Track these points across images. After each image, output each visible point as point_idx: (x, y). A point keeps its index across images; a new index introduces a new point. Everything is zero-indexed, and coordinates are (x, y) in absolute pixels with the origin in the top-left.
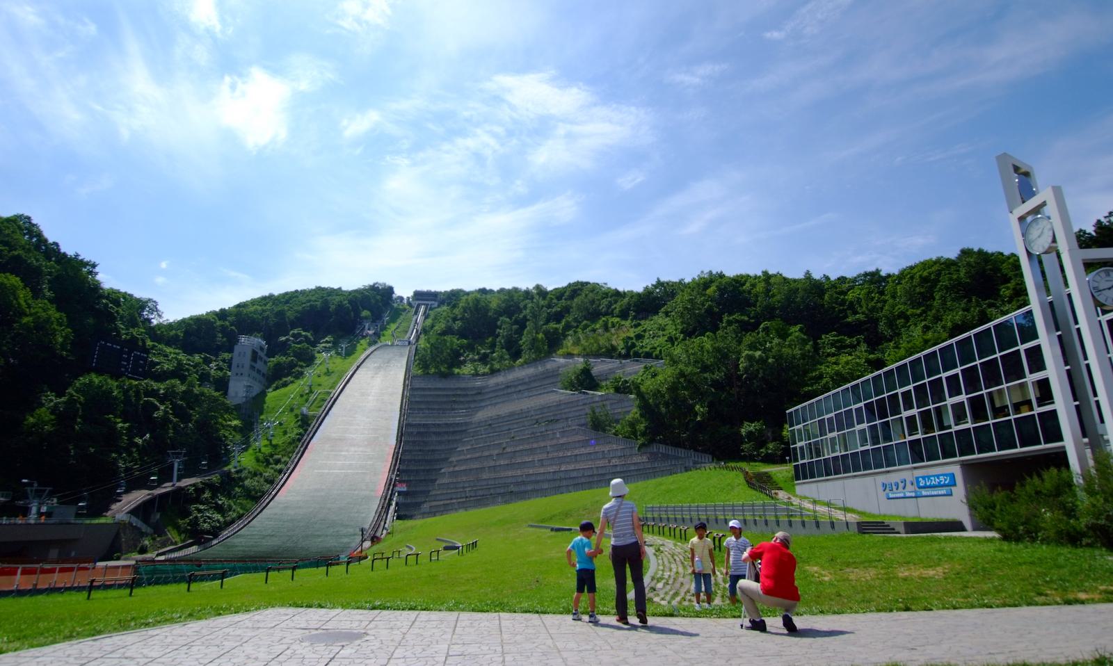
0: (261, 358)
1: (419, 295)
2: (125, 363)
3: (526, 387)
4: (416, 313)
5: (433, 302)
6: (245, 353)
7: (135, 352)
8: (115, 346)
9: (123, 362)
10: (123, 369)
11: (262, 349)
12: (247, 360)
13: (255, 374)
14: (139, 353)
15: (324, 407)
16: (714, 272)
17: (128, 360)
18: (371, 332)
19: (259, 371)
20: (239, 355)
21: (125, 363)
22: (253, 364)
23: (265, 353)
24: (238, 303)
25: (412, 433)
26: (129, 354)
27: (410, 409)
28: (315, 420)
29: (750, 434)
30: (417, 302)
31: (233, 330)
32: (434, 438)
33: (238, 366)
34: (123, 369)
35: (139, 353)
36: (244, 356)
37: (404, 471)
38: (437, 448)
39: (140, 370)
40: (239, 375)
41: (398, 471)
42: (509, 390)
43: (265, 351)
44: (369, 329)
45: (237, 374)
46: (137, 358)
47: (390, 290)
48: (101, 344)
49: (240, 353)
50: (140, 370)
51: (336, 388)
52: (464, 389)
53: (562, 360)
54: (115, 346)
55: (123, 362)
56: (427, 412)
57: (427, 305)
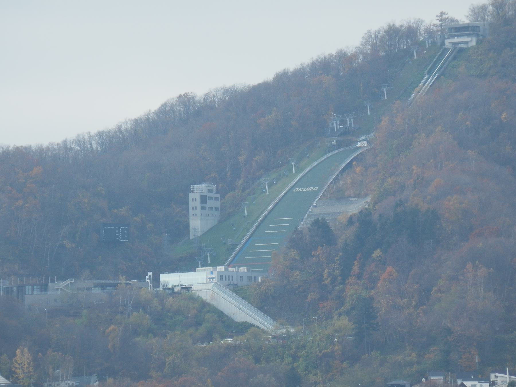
2: (118, 235)
6: (196, 199)
9: (117, 235)
10: (118, 238)
21: (118, 235)
22: (204, 205)
34: (118, 238)
45: (193, 215)
55: (117, 235)
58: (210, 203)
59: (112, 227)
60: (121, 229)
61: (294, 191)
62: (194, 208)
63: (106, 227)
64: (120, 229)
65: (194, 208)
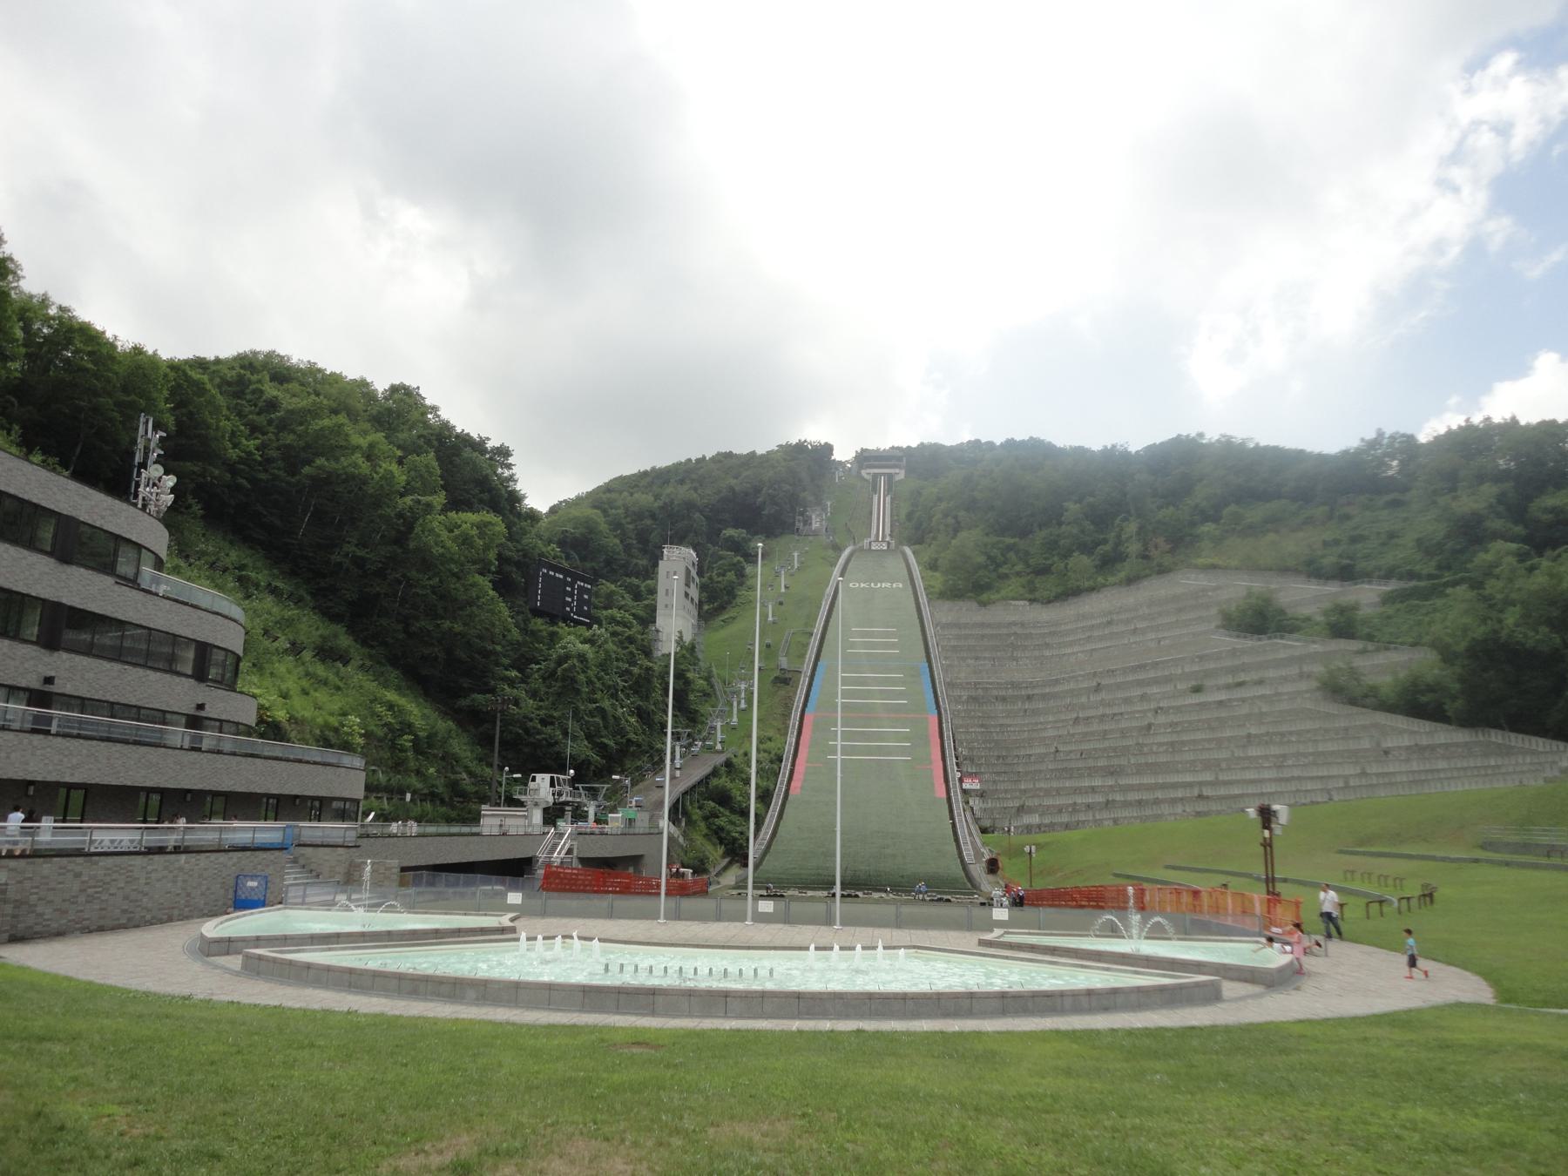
2: (570, 600)
5: (897, 471)
8: (552, 573)
10: (568, 609)
17: (571, 595)
25: (960, 697)
34: (568, 609)
42: (1115, 629)
56: (973, 661)
59: (560, 573)
61: (851, 585)
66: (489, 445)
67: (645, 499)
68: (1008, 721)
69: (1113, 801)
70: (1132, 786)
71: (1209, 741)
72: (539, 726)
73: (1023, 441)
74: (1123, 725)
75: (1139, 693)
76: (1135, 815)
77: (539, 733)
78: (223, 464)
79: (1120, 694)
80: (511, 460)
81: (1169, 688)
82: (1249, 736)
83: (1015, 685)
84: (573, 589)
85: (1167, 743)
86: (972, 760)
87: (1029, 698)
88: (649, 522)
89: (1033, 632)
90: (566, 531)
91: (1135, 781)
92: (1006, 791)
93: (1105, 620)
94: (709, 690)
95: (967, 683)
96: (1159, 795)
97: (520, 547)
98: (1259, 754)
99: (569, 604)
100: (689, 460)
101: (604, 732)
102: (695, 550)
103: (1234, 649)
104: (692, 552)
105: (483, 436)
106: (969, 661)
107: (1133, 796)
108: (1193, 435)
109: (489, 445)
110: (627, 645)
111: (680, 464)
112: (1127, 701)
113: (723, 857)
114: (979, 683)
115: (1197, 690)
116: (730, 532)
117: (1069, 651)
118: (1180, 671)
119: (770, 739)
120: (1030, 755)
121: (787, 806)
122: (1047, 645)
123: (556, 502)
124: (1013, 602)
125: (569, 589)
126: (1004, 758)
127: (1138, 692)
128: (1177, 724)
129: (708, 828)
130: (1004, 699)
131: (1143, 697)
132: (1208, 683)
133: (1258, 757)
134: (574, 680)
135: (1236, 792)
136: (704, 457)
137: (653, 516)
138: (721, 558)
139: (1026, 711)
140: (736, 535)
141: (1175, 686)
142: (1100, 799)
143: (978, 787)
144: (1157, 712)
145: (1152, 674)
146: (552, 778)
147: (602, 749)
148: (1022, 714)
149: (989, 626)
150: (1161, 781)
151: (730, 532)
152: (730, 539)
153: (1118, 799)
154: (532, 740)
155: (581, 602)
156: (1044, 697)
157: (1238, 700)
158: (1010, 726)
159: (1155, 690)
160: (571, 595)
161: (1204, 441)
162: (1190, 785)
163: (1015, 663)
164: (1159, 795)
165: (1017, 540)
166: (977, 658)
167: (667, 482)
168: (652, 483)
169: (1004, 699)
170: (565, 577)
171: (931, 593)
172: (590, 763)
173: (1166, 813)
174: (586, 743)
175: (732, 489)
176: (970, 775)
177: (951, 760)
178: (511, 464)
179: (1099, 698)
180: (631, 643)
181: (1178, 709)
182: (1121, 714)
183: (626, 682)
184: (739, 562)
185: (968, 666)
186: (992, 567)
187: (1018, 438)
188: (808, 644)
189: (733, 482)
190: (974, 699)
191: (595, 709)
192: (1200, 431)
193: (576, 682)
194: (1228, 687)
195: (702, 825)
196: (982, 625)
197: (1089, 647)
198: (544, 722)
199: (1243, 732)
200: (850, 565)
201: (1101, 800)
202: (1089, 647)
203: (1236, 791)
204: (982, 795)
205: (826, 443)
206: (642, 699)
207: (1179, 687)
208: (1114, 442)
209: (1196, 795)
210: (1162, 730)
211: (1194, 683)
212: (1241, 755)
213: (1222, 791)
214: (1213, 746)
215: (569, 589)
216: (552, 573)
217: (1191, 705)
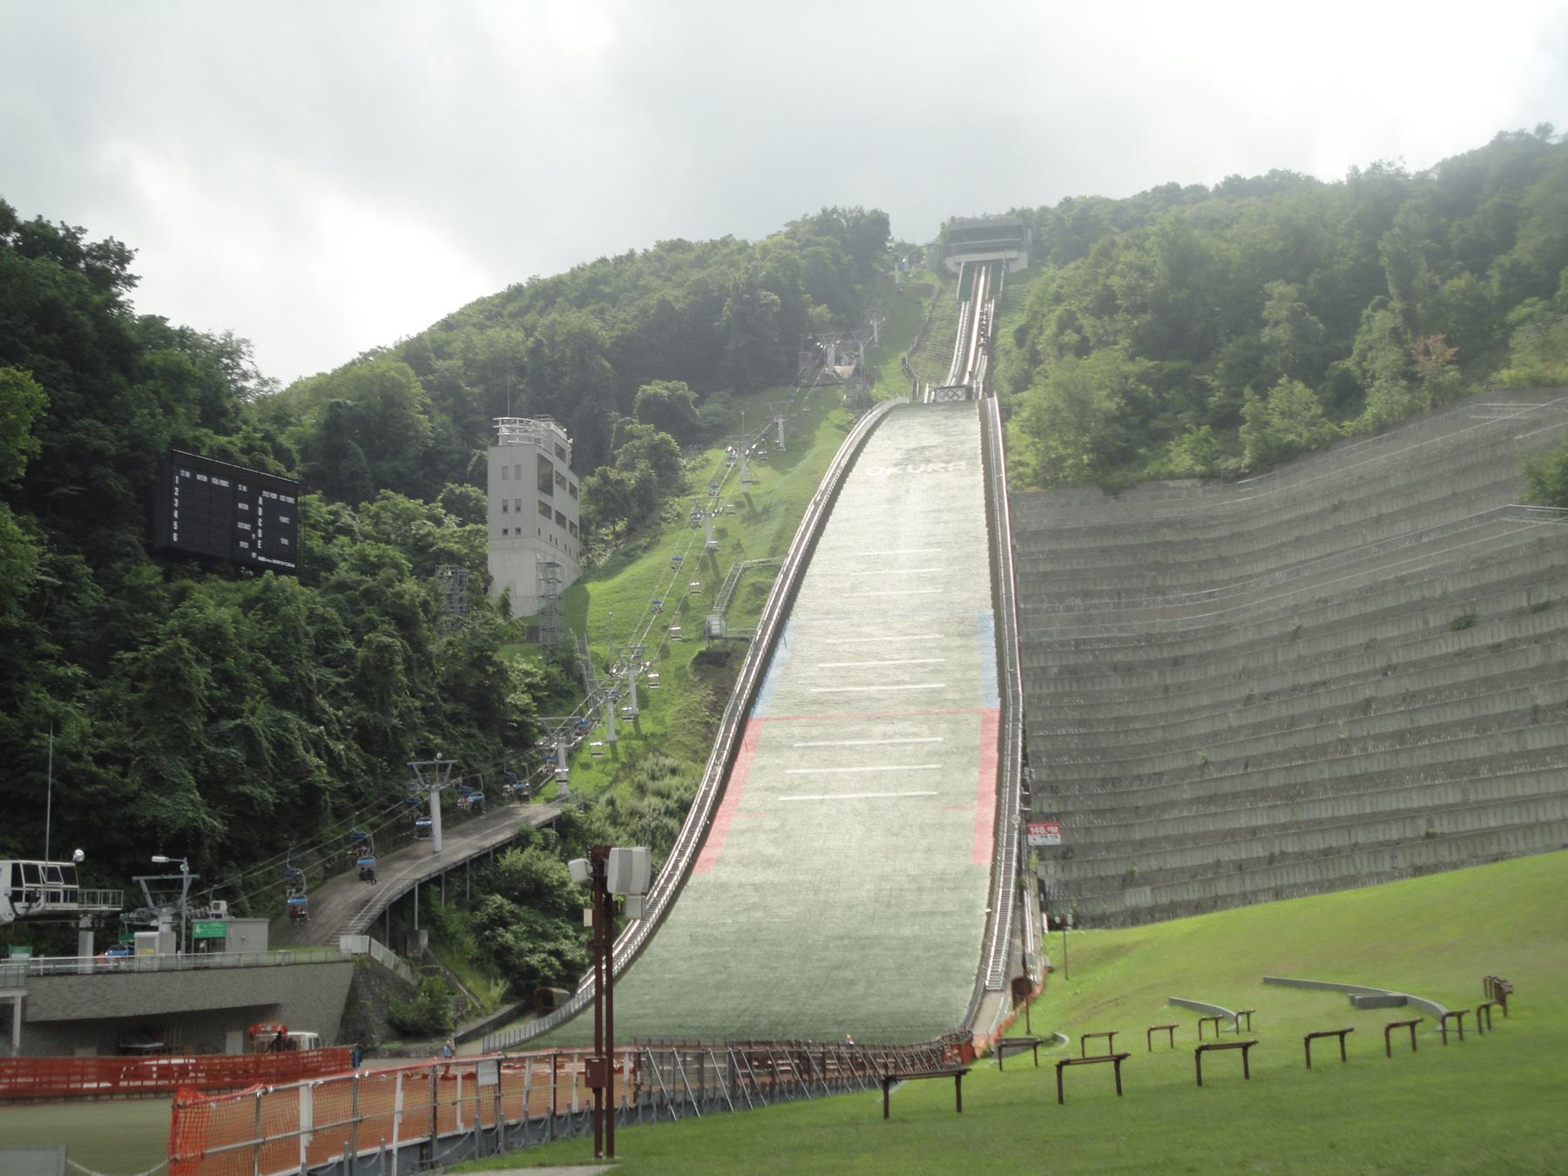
0: (562, 481)
1: (961, 236)
2: (247, 527)
3: (1397, 505)
4: (967, 293)
5: (1013, 254)
6: (518, 467)
7: (265, 493)
8: (202, 478)
10: (244, 544)
11: (560, 453)
12: (528, 490)
13: (551, 526)
14: (274, 496)
15: (766, 611)
16: (1362, 170)
17: (251, 517)
18: (844, 370)
19: (561, 519)
20: (505, 478)
21: (247, 527)
22: (546, 499)
23: (568, 462)
24: (443, 316)
25: (1044, 669)
26: (251, 500)
27: (1026, 598)
28: (750, 652)
29: (1519, 440)
30: (964, 259)
31: (667, 442)
32: (1117, 683)
33: (505, 509)
34: (244, 544)
35: (274, 496)
36: (518, 476)
37: (1042, 787)
38: (1131, 712)
39: (285, 541)
40: (512, 532)
41: (1025, 785)
42: (1342, 519)
43: (568, 457)
44: (838, 361)
45: (505, 531)
46: (273, 508)
47: (878, 224)
48: (182, 479)
49: (505, 468)
50: (285, 541)
51: (791, 552)
52: (1183, 524)
53: (1515, 411)
54: (215, 481)
56: (1078, 601)
57: (995, 267)
58: (560, 500)
59: (220, 477)
60: (265, 499)
62: (511, 473)
63: (186, 469)
64: (260, 502)
65: (511, 473)
66: (86, 241)
67: (509, 337)
68: (1131, 711)
69: (1283, 853)
70: (1320, 822)
71: (1465, 724)
72: (94, 769)
73: (1258, 178)
74: (1324, 703)
75: (1362, 641)
76: (1311, 879)
77: (93, 779)
78: (1309, 450)
79: (1329, 645)
80: (130, 269)
81: (1414, 625)
82: (1536, 710)
83: (1152, 640)
84: (254, 506)
85: (1392, 735)
86: (1054, 789)
87: (1176, 663)
88: (512, 378)
89: (1199, 536)
90: (338, 404)
91: (1347, 809)
92: (1109, 846)
93: (1328, 504)
94: (571, 684)
95: (1062, 644)
96: (1361, 837)
97: (126, 431)
98: (1546, 744)
99: (246, 536)
100: (604, 261)
101: (249, 773)
102: (560, 422)
103: (1541, 540)
104: (553, 426)
105: (71, 225)
106: (1073, 601)
107: (1316, 843)
108: (1531, 129)
109: (86, 241)
110: (363, 605)
111: (581, 269)
112: (1340, 655)
113: (505, 1000)
114: (1084, 641)
115: (1466, 624)
116: (657, 388)
117: (1259, 568)
118: (1438, 593)
119: (674, 771)
120: (1161, 774)
121: (683, 894)
122: (1223, 561)
123: (356, 356)
124: (1171, 483)
125: (243, 506)
126: (1114, 781)
127: (1358, 638)
128: (1414, 696)
129: (481, 945)
130: (1129, 669)
131: (1370, 647)
132: (1484, 611)
133: (1547, 751)
134: (176, 676)
135: (1493, 823)
136: (632, 253)
137: (521, 370)
138: (632, 436)
139: (1166, 689)
140: (666, 393)
141: (1426, 622)
142: (1258, 850)
143: (1058, 841)
144: (1385, 674)
145: (1389, 602)
146: (16, 868)
147: (242, 810)
148: (1160, 695)
149: (1118, 531)
150: (1368, 810)
151: (657, 388)
152: (652, 402)
153: (1290, 849)
154: (78, 796)
155: (273, 529)
156: (1204, 658)
157: (1528, 640)
158: (1134, 719)
159: (1389, 631)
160: (251, 517)
161: (1554, 141)
162: (1412, 815)
163: (1159, 598)
164: (1361, 837)
165: (1186, 363)
166: (1086, 594)
167: (551, 302)
168: (523, 312)
169: (1129, 669)
170: (234, 485)
171: (1020, 477)
172: (198, 833)
173: (1365, 870)
174: (197, 796)
175: (664, 304)
176: (1047, 819)
177: (1013, 792)
178: (131, 277)
179: (1294, 656)
180: (371, 603)
181: (1422, 666)
182: (1324, 683)
183: (345, 675)
184: (663, 441)
185: (1069, 609)
186: (1135, 420)
187: (1248, 175)
188: (770, 587)
189: (671, 293)
190: (1071, 672)
191: (232, 730)
192: (1543, 121)
193: (183, 679)
194: (1519, 614)
195: (470, 941)
196: (1105, 530)
197: (1293, 558)
198: (102, 759)
199: (1523, 705)
200: (877, 433)
201: (1261, 854)
202: (1293, 558)
203: (1492, 821)
204: (1063, 855)
205: (875, 211)
206: (371, 707)
207: (1432, 623)
208: (1375, 159)
209: (1423, 833)
210: (1389, 710)
211: (1459, 613)
212: (1516, 749)
213: (1469, 823)
214: (1470, 735)
215: (243, 506)
216: (202, 478)
217: (1445, 657)
